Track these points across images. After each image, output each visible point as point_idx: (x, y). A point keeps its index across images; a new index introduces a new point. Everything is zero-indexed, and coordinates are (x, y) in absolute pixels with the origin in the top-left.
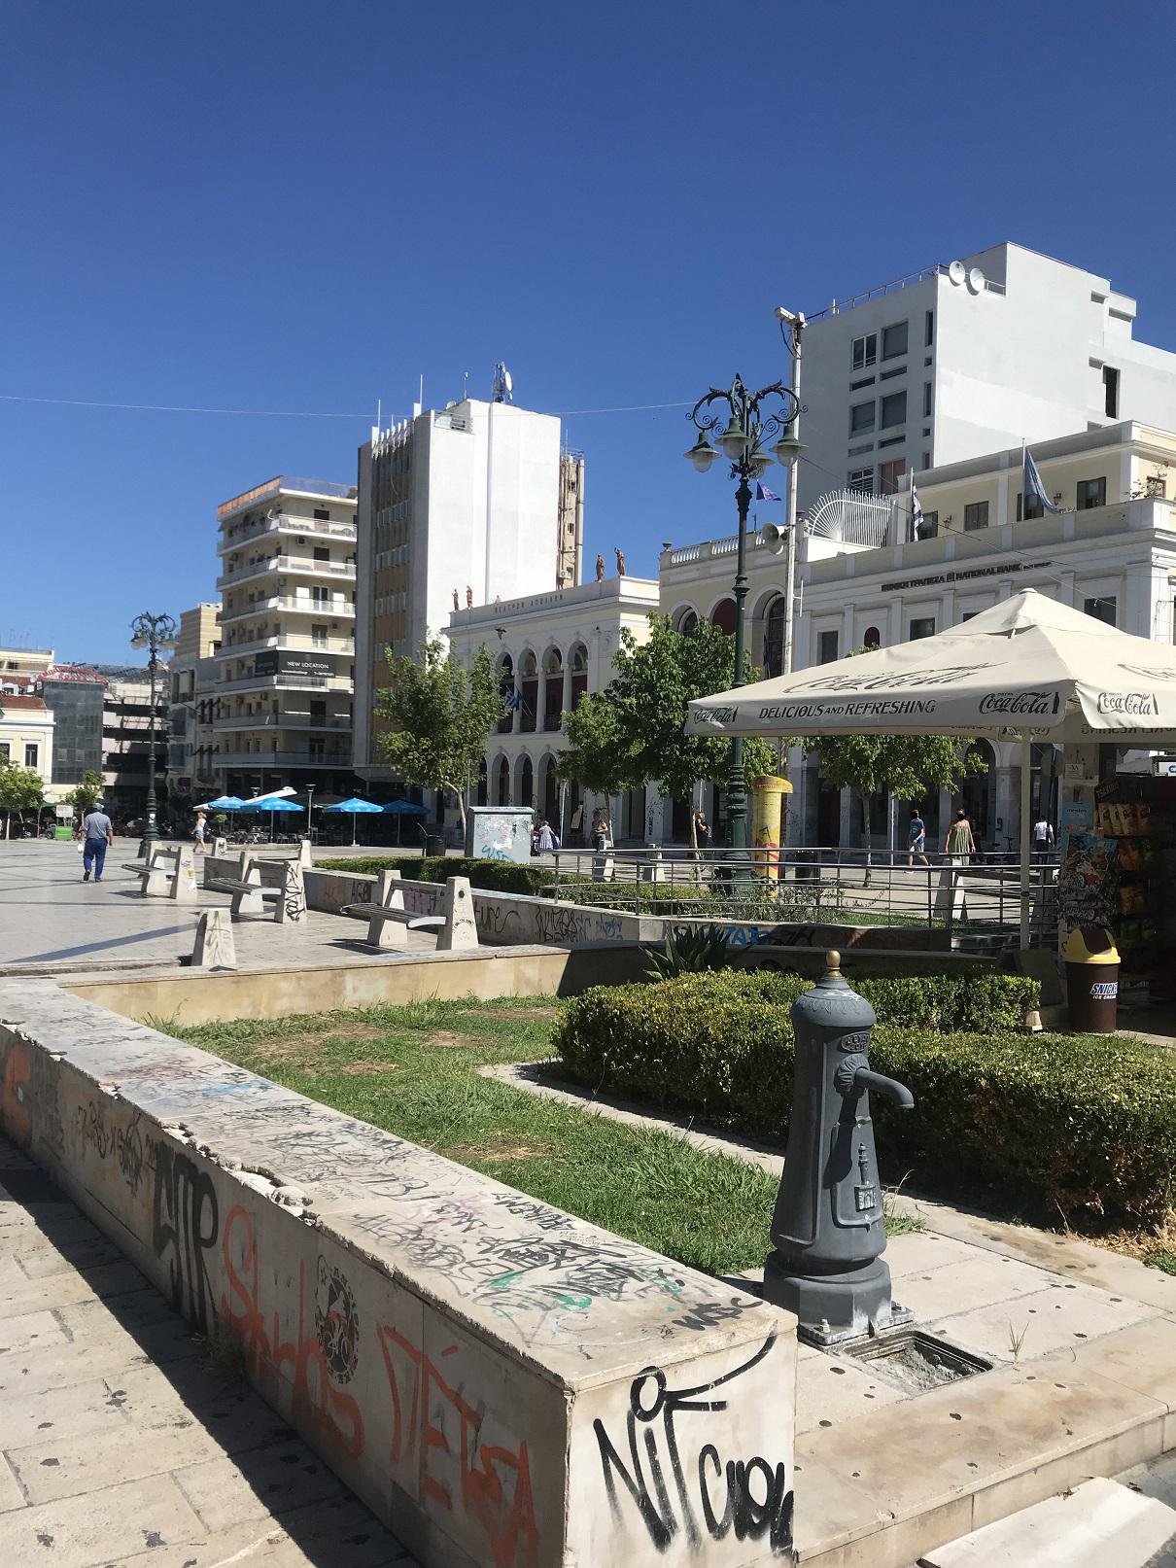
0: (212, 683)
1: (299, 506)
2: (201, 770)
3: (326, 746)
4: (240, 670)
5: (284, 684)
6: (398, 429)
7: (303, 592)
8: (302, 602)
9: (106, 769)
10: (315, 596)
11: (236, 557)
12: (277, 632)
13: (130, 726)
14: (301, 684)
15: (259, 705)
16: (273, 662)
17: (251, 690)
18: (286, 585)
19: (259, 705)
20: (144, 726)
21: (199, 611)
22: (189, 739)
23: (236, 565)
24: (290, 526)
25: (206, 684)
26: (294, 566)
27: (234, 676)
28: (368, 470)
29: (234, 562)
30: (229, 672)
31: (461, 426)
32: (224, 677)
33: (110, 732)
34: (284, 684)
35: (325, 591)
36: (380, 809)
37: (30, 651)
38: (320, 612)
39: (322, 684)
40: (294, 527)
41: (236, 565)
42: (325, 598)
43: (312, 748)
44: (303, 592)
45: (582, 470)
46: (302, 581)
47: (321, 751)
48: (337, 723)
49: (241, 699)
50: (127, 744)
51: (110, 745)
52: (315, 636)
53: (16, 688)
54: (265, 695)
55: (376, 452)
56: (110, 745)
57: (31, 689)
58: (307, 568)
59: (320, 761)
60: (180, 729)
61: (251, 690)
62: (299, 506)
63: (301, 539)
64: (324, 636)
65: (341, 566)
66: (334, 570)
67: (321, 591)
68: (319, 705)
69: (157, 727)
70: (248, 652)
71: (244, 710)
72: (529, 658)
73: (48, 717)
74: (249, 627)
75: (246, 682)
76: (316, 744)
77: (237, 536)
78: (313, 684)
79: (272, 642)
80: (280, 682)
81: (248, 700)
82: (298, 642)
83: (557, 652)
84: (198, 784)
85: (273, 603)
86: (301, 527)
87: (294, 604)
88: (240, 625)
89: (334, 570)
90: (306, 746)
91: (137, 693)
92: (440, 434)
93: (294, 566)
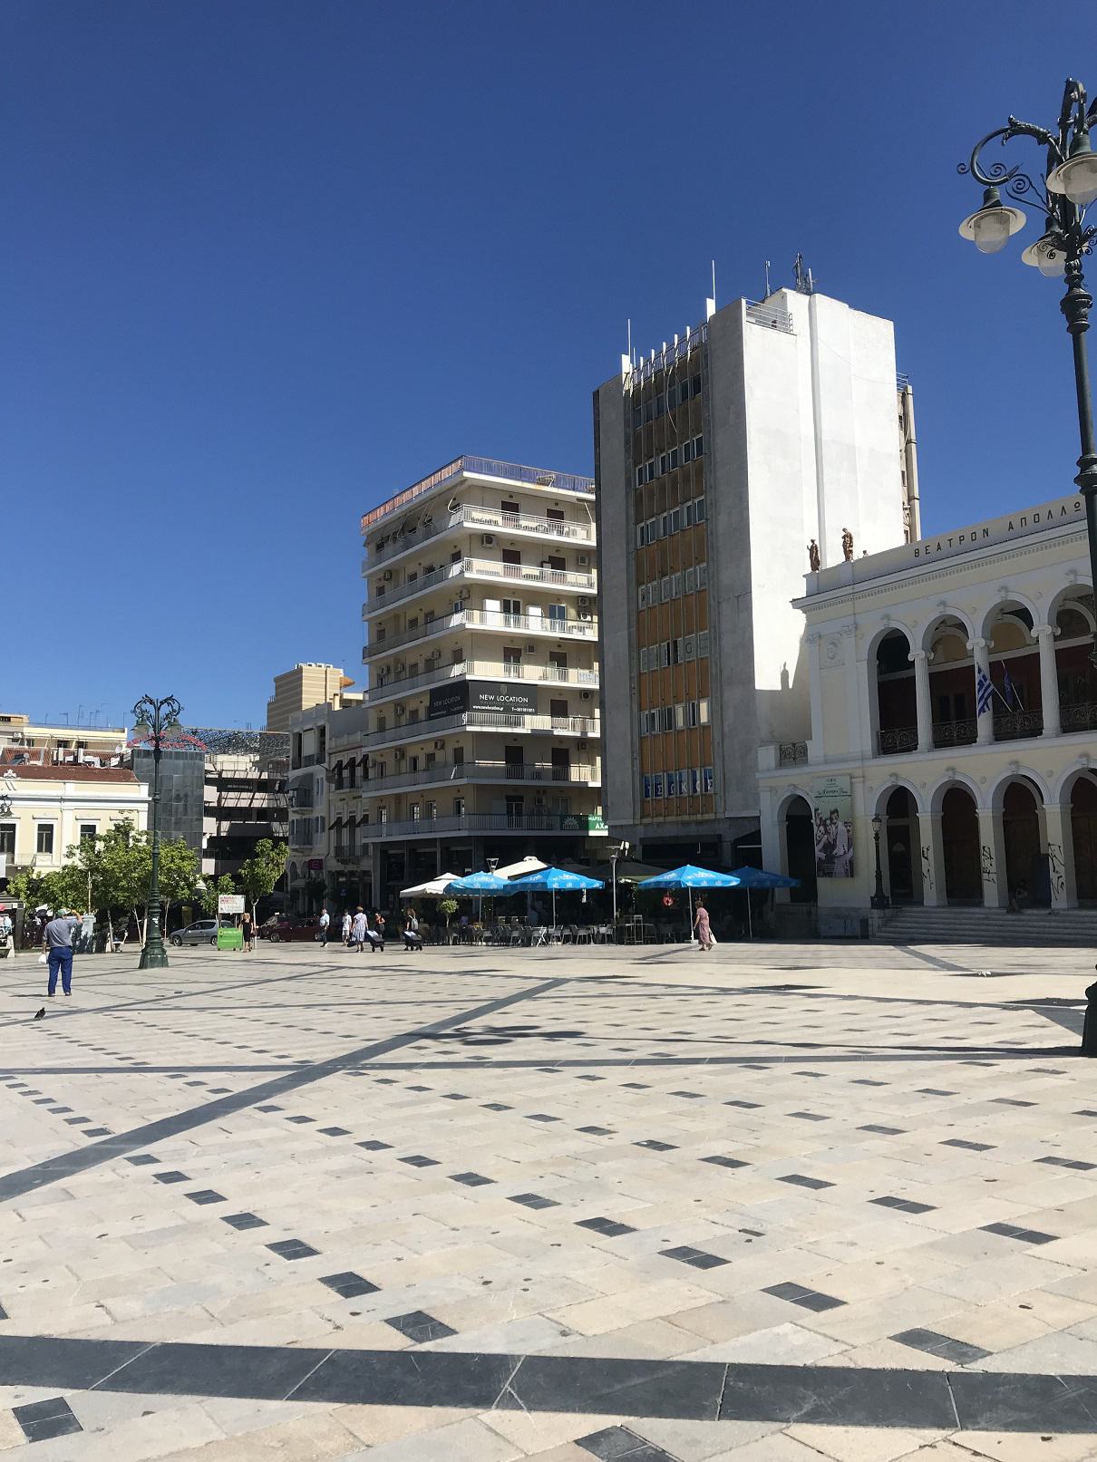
0: (358, 737)
1: (484, 495)
2: (339, 849)
3: (526, 806)
4: (398, 716)
5: (480, 723)
6: (678, 344)
7: (493, 605)
8: (491, 618)
9: (207, 854)
10: (506, 608)
11: (390, 574)
12: (458, 658)
13: (230, 803)
14: (496, 724)
15: (431, 757)
16: (461, 696)
17: (419, 740)
18: (472, 595)
19: (431, 757)
20: (244, 804)
21: (300, 670)
22: (319, 810)
23: (388, 587)
24: (473, 520)
25: (345, 740)
26: (479, 571)
27: (390, 723)
28: (614, 418)
29: (384, 584)
30: (382, 721)
31: (779, 322)
32: (373, 726)
33: (210, 812)
34: (480, 723)
35: (517, 605)
36: (733, 881)
37: (95, 728)
38: (512, 629)
39: (517, 724)
40: (481, 521)
41: (388, 587)
42: (517, 611)
43: (509, 807)
44: (493, 605)
45: (1089, 339)
46: (490, 590)
47: (519, 814)
48: (538, 775)
49: (400, 752)
50: (225, 825)
51: (210, 826)
52: (506, 660)
53: (97, 760)
54: (440, 744)
55: (628, 386)
56: (210, 826)
57: (115, 761)
58: (497, 574)
59: (519, 825)
60: (305, 796)
61: (419, 740)
62: (484, 495)
63: (488, 538)
64: (517, 661)
65: (535, 571)
66: (528, 577)
67: (513, 604)
68: (515, 750)
69: (256, 804)
70: (417, 692)
71: (406, 765)
72: (948, 632)
73: (143, 791)
74: (410, 660)
75: (403, 730)
76: (514, 801)
77: (388, 549)
78: (508, 723)
79: (457, 670)
80: (471, 723)
81: (411, 753)
82: (487, 670)
83: (1024, 615)
84: (333, 865)
85: (456, 619)
86: (489, 522)
87: (482, 620)
88: (397, 659)
89: (528, 577)
90: (501, 806)
91: (238, 764)
92: (755, 339)
93: (479, 571)
